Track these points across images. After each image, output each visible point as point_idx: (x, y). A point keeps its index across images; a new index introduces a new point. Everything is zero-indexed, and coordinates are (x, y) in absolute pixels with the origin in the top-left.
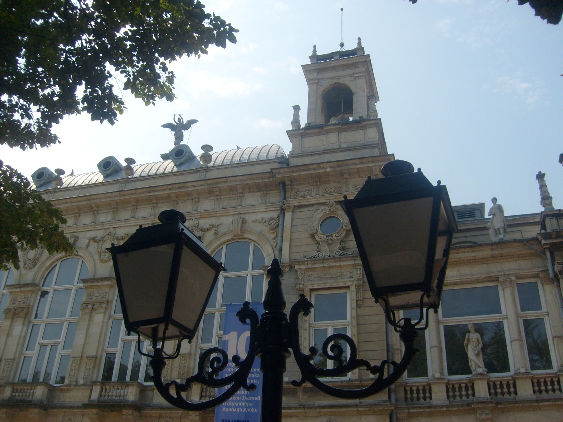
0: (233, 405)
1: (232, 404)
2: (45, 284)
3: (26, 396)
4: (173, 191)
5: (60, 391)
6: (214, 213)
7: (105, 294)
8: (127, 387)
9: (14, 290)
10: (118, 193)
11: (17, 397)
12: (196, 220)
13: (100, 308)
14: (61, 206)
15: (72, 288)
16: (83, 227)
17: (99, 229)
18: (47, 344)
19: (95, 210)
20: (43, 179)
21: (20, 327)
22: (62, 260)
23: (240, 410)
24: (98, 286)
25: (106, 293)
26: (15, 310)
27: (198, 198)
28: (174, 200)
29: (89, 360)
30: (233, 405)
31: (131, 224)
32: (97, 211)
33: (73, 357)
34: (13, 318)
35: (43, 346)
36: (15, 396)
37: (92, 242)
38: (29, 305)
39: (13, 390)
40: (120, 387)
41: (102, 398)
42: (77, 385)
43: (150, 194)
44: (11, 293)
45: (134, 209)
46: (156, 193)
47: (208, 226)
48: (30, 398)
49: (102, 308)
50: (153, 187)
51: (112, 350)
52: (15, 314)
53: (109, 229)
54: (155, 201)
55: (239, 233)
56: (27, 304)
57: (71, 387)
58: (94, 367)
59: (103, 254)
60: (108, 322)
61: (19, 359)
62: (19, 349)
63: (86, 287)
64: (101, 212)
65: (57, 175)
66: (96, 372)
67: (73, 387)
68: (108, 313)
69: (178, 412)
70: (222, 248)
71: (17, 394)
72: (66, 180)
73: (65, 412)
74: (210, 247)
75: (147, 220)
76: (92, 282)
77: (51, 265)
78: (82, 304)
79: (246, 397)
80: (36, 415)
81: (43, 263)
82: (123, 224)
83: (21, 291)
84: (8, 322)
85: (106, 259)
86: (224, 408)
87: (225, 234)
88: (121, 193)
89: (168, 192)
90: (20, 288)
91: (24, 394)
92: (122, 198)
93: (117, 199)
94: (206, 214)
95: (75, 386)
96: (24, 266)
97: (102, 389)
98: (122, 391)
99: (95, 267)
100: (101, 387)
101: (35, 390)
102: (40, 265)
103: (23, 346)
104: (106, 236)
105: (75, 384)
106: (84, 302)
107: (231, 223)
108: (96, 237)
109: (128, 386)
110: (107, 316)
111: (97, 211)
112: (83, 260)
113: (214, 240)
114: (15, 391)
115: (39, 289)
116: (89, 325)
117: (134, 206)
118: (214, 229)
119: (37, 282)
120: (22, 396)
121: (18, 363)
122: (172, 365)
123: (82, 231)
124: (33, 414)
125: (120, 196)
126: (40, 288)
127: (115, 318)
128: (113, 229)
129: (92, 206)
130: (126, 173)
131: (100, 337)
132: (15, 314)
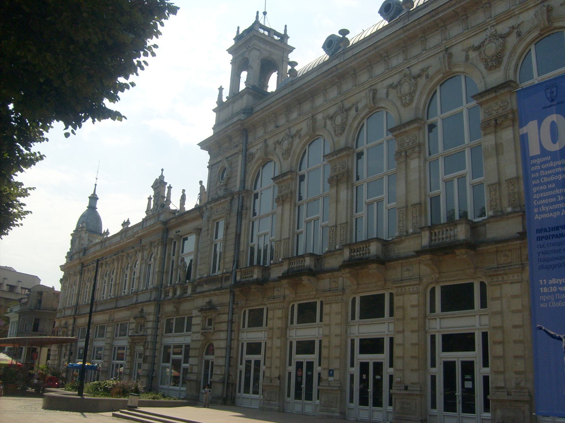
0: (547, 209)
1: (545, 208)
2: (359, 143)
3: (363, 254)
4: (458, 6)
5: (394, 244)
6: (511, 12)
7: (415, 138)
8: (455, 227)
9: (331, 159)
10: (402, 30)
11: (355, 256)
12: (492, 28)
13: (413, 153)
14: (353, 64)
15: (383, 141)
16: (378, 78)
17: (394, 75)
18: (373, 201)
19: (385, 57)
20: (333, 47)
21: (345, 192)
22: (367, 117)
23: (558, 213)
24: (406, 132)
25: (416, 137)
26: (337, 177)
27: (489, 3)
28: (462, 16)
29: (414, 208)
30: (547, 209)
31: (425, 58)
32: (388, 56)
33: (398, 209)
34: (337, 185)
35: (369, 204)
36: (354, 256)
37: (390, 89)
38: (348, 169)
39: (351, 251)
40: (448, 228)
41: (433, 243)
42: (407, 234)
43: (435, 18)
44: (329, 162)
45: (422, 41)
46: (441, 15)
47: (507, 30)
48: (367, 255)
49: (415, 152)
50: (435, 9)
51: (434, 192)
52: (338, 181)
53: (403, 71)
54: (442, 24)
55: (547, 24)
56: (346, 168)
57: (402, 238)
58: (420, 215)
59: (403, 98)
60: (424, 166)
61: (352, 223)
62: (349, 212)
63: (395, 136)
64: (391, 56)
65: (341, 36)
66: (423, 219)
67: (404, 238)
68: (422, 155)
69: (516, 242)
70: (530, 50)
71: (355, 254)
72: (353, 38)
73: (402, 263)
74: (515, 53)
75: (439, 48)
76: (400, 129)
77: (359, 125)
78: (395, 154)
79: (562, 197)
80: (375, 270)
81: (351, 126)
82: (415, 61)
83: (338, 158)
84: (334, 190)
85: (407, 102)
86: (537, 215)
87: (529, 32)
88: (405, 29)
89: (453, 8)
90: (336, 155)
91: (361, 252)
92: (406, 34)
93: (402, 36)
94: (502, 17)
95: (406, 236)
96: (335, 134)
97: (431, 233)
98: (452, 232)
99: (399, 114)
100: (430, 231)
101: (370, 247)
102: (348, 129)
103: (352, 208)
104: (402, 78)
105: (405, 234)
106: (396, 152)
107: (534, 16)
108: (393, 83)
109: (456, 225)
110: (422, 159)
111: (388, 56)
112: (387, 110)
113: (519, 43)
114: (353, 251)
115: (354, 152)
116: (406, 173)
117: (421, 37)
118: (515, 31)
119: (350, 145)
120: (360, 255)
121: (352, 226)
122: (500, 193)
123: (379, 82)
124: (372, 269)
125: (405, 32)
126: (354, 150)
127: (431, 159)
128: (407, 69)
129: (381, 53)
130: (406, 7)
131: (420, 182)
132: (338, 181)
